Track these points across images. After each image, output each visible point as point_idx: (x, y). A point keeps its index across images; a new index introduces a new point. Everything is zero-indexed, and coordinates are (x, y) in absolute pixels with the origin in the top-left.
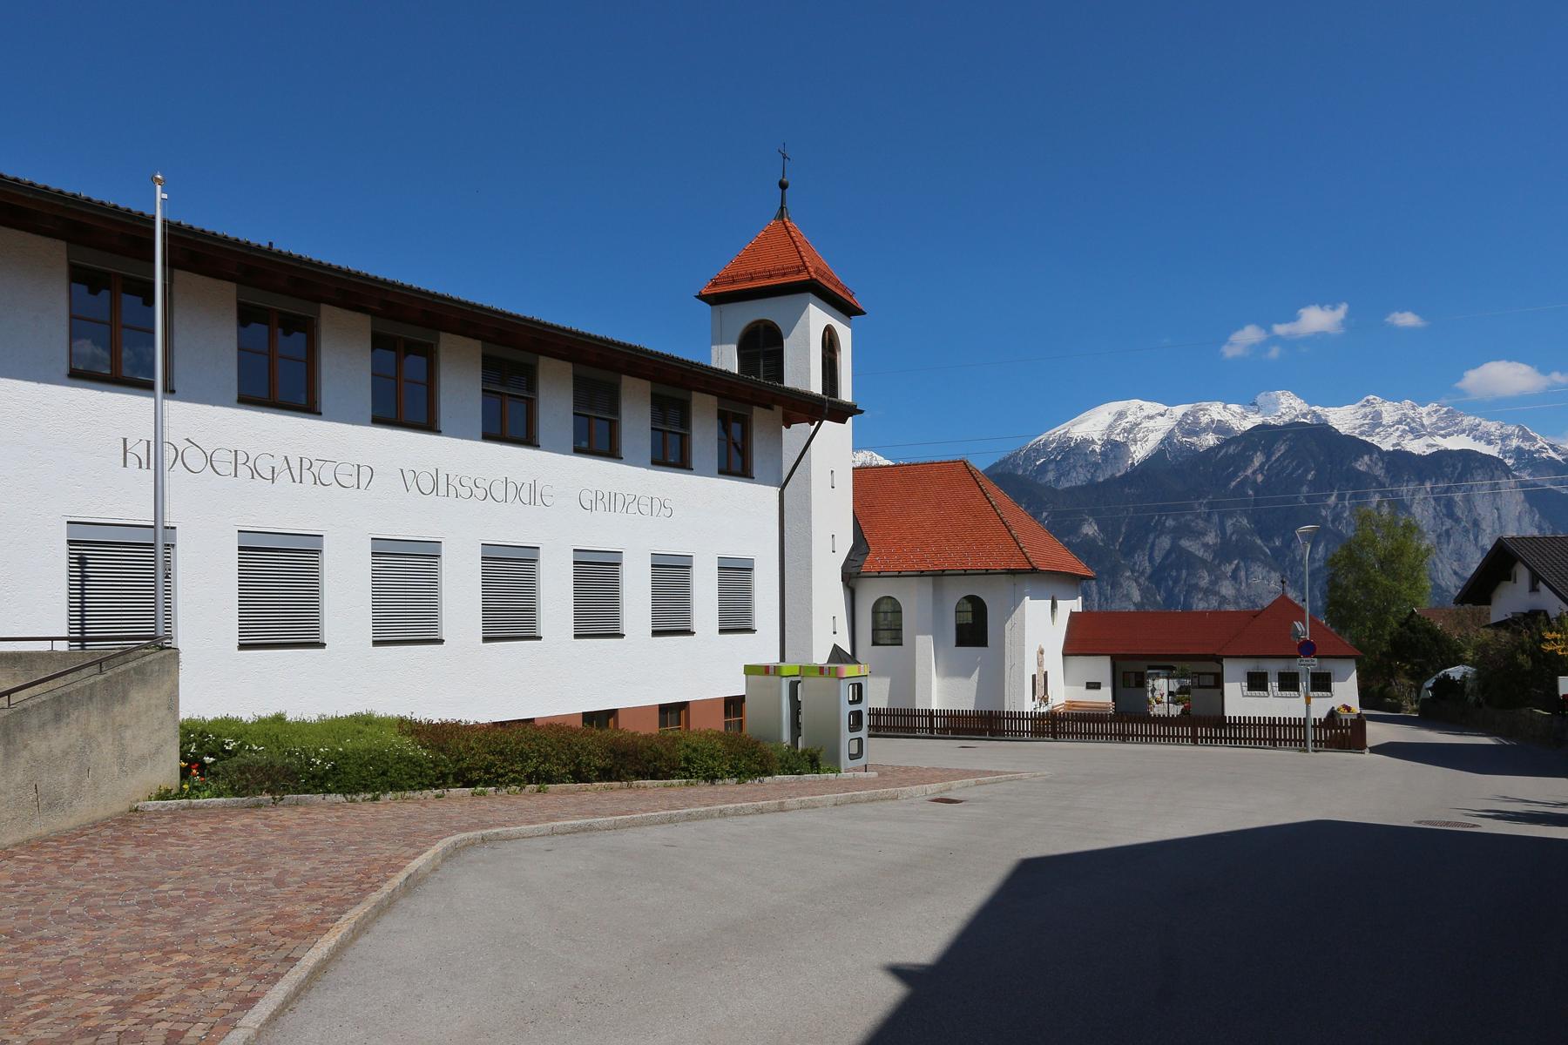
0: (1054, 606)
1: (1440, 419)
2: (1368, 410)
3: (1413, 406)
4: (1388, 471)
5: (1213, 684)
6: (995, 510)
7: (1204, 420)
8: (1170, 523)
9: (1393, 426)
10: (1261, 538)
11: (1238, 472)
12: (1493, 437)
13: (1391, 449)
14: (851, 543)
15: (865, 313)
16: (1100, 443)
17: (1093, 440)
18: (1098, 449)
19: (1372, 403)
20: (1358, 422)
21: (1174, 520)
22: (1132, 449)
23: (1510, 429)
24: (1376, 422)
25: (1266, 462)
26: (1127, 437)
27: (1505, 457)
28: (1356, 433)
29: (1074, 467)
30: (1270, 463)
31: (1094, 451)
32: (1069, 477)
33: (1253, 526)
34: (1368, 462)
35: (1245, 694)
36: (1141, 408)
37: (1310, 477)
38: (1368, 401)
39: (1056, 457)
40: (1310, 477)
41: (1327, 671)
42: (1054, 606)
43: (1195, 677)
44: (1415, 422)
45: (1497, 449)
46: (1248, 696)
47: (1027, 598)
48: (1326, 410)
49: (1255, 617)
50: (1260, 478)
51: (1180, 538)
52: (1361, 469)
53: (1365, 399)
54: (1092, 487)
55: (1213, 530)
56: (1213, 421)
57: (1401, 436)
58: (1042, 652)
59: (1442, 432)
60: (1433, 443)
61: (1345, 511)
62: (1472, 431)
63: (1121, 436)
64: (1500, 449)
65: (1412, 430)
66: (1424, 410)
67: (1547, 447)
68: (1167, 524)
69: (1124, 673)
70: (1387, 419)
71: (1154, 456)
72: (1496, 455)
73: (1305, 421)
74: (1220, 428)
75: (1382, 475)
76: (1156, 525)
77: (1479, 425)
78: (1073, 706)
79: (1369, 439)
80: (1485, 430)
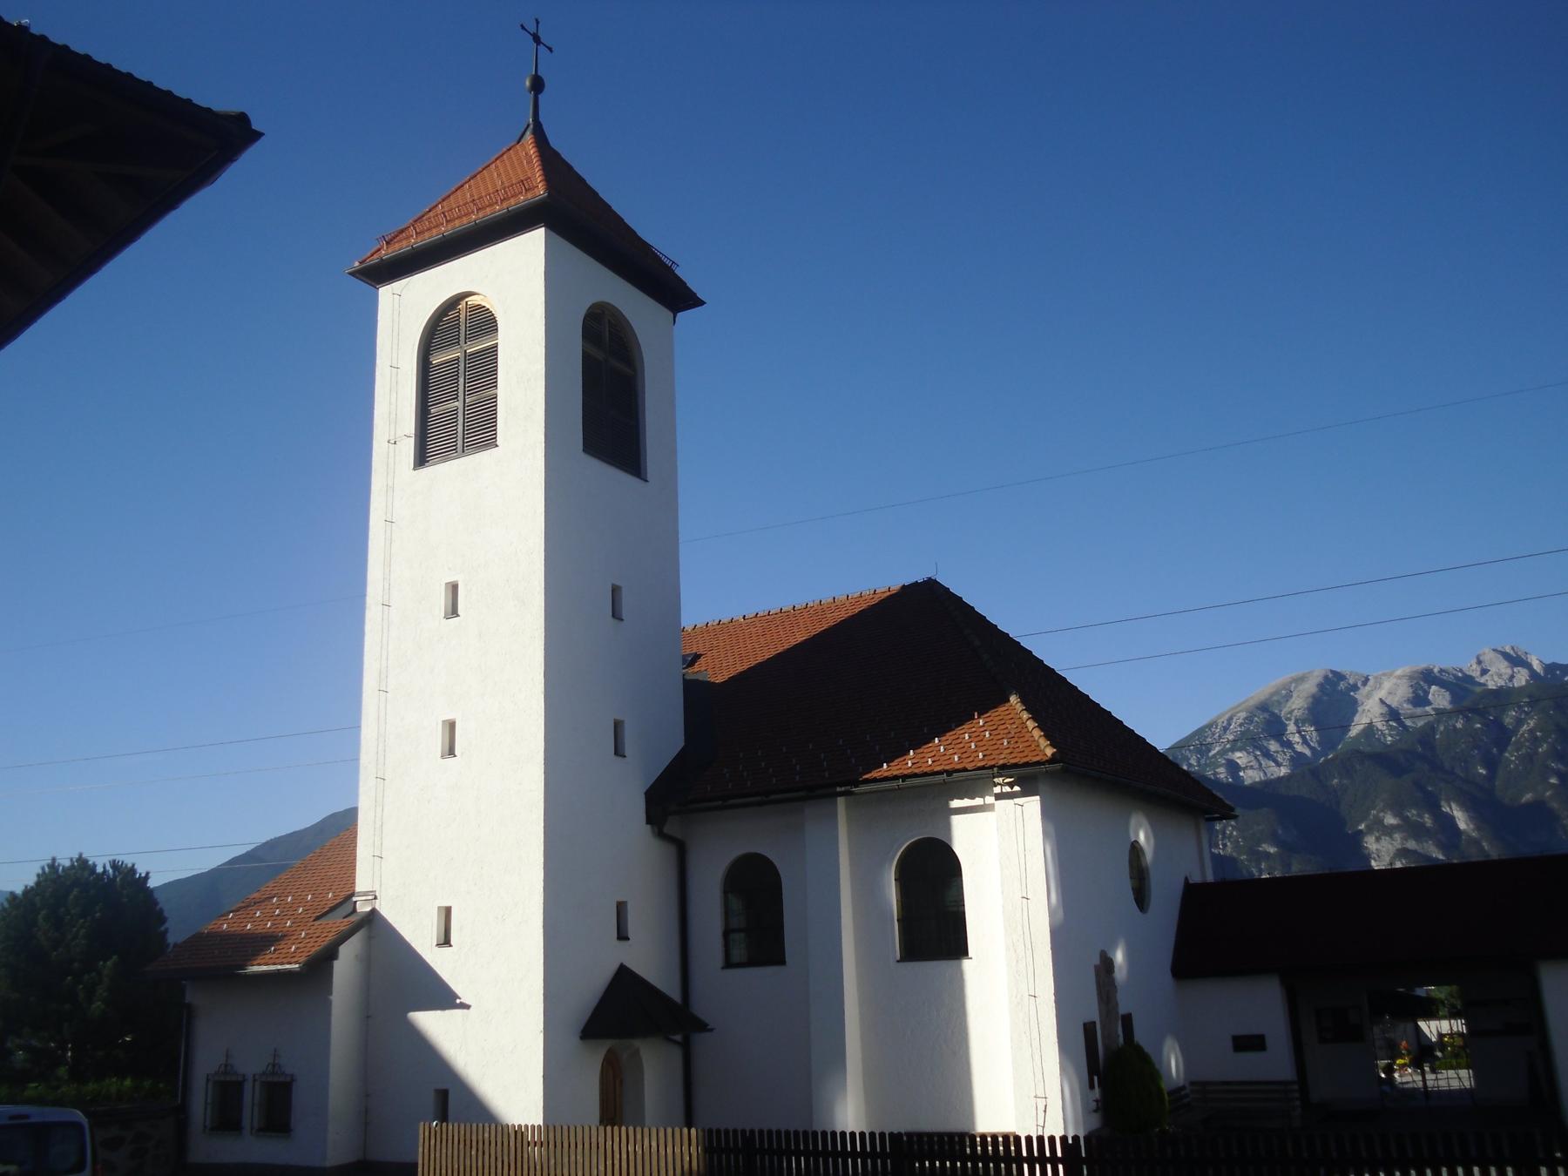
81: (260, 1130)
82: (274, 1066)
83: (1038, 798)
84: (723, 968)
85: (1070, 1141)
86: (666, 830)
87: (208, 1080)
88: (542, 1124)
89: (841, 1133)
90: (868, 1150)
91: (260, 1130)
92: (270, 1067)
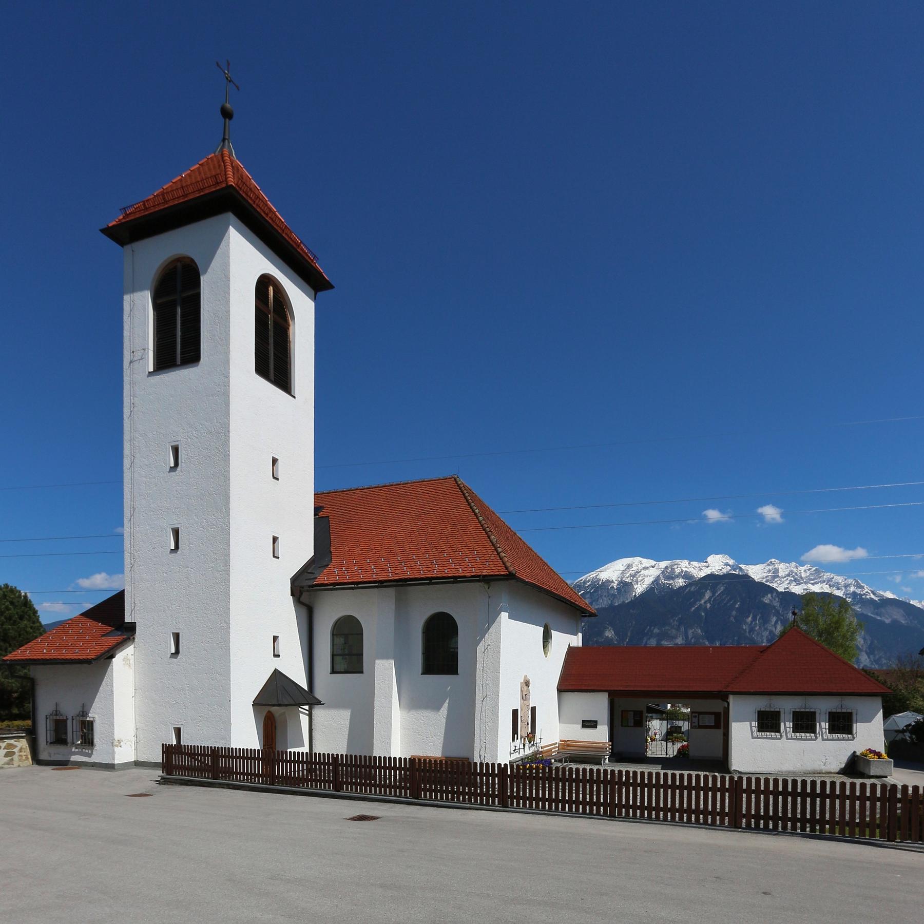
0: (547, 637)
1: (811, 574)
2: (771, 567)
3: (796, 566)
4: (781, 604)
5: (713, 724)
6: (478, 518)
7: (677, 571)
8: (656, 631)
9: (785, 577)
10: (708, 641)
11: (696, 602)
12: (840, 586)
13: (784, 591)
14: (311, 553)
15: (332, 287)
16: (616, 582)
17: (612, 581)
18: (615, 585)
19: (774, 564)
20: (765, 575)
21: (659, 629)
22: (635, 587)
23: (850, 581)
24: (775, 575)
25: (713, 596)
26: (632, 580)
27: (847, 597)
28: (764, 580)
29: (601, 596)
30: (714, 597)
31: (613, 587)
32: (598, 602)
33: (704, 634)
34: (771, 598)
35: (755, 735)
36: (641, 563)
37: (737, 606)
38: (771, 562)
39: (590, 590)
40: (737, 606)
41: (848, 711)
42: (547, 637)
43: (695, 717)
44: (797, 575)
45: (842, 592)
46: (757, 738)
47: (504, 615)
48: (747, 566)
49: (761, 652)
50: (708, 606)
51: (662, 640)
52: (766, 602)
53: (770, 561)
54: (612, 608)
55: (681, 636)
56: (682, 571)
57: (789, 583)
58: (527, 684)
59: (812, 582)
60: (806, 587)
61: (756, 627)
62: (829, 582)
63: (629, 578)
64: (844, 592)
65: (795, 580)
66: (802, 569)
67: (870, 592)
68: (654, 632)
69: (622, 711)
70: (781, 573)
71: (647, 591)
72: (842, 596)
73: (735, 573)
74: (686, 576)
75: (778, 606)
76: (648, 631)
77: (833, 578)
78: (568, 745)
79: (770, 585)
80: (836, 581)
81: (51, 743)
82: (56, 711)
83: (580, 645)
84: (330, 674)
85: (335, 756)
86: (302, 599)
87: (47, 718)
88: (308, 752)
89: (379, 757)
90: (305, 760)
91: (51, 743)
92: (54, 712)
